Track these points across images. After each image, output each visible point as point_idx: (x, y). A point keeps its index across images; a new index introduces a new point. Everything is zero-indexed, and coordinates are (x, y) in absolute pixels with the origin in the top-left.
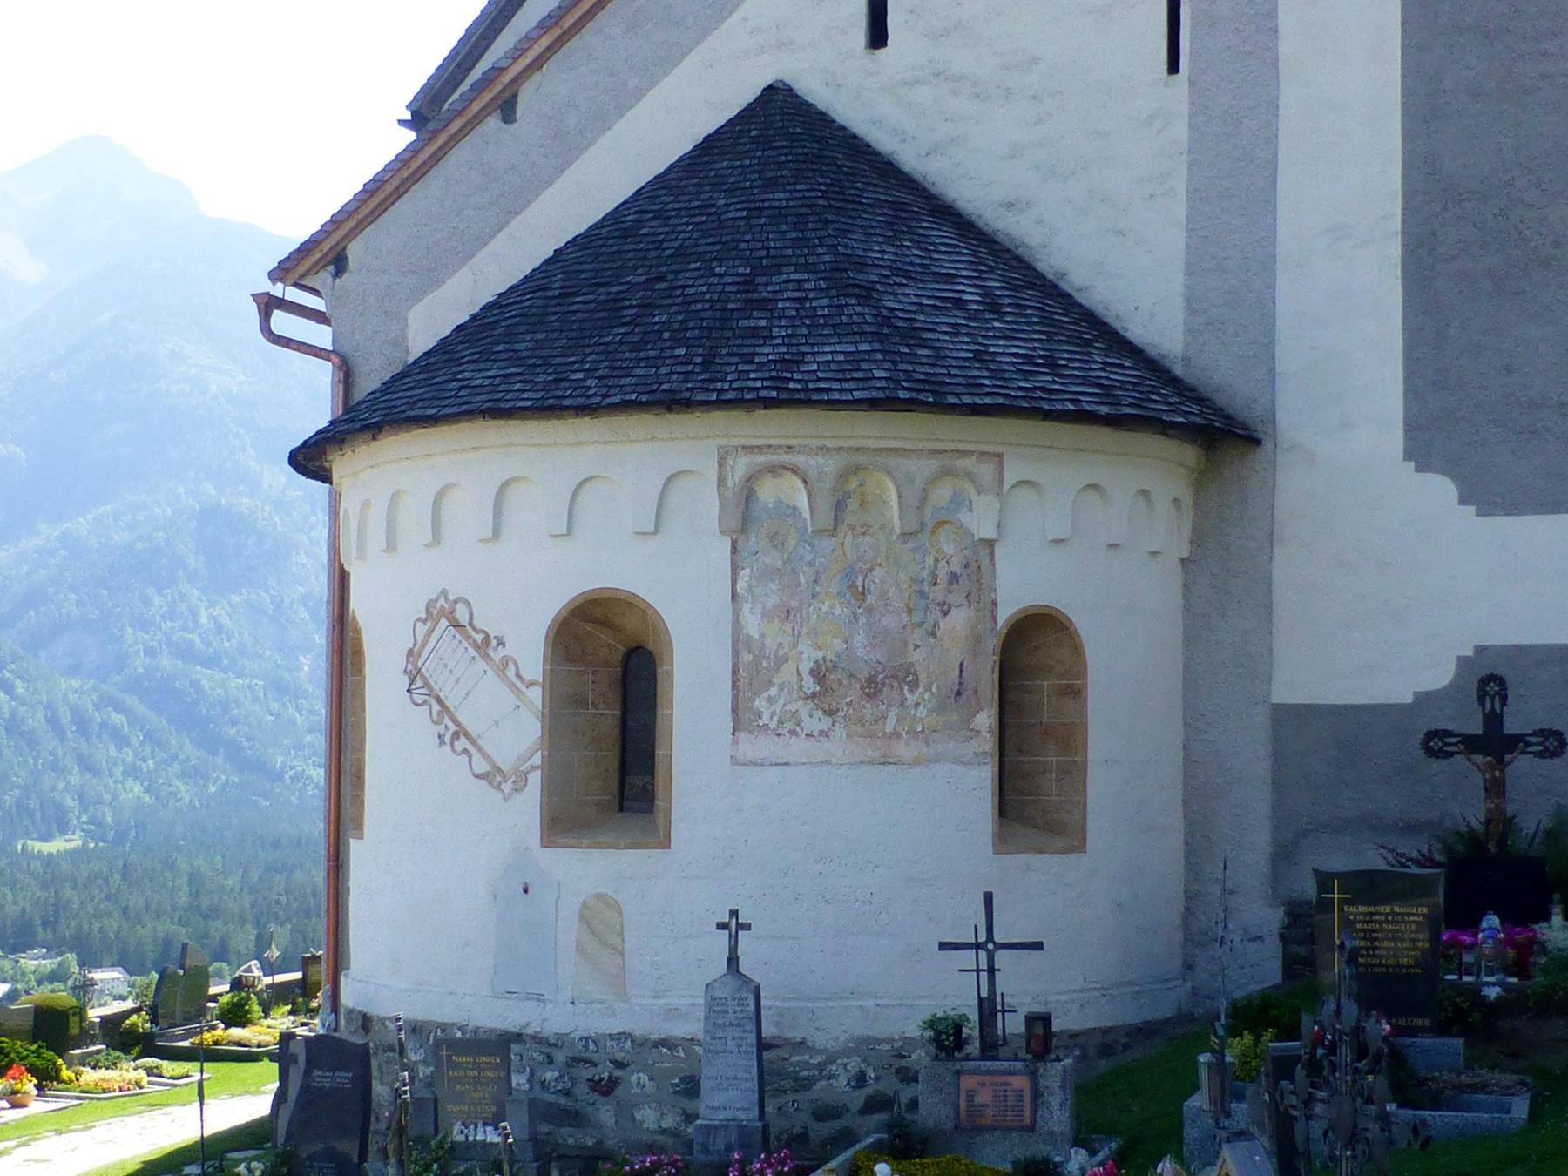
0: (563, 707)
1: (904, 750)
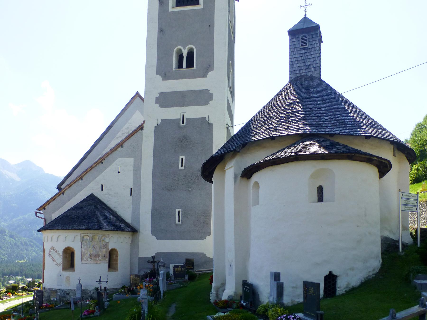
0: (64, 258)
1: (99, 262)
